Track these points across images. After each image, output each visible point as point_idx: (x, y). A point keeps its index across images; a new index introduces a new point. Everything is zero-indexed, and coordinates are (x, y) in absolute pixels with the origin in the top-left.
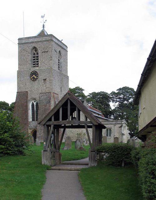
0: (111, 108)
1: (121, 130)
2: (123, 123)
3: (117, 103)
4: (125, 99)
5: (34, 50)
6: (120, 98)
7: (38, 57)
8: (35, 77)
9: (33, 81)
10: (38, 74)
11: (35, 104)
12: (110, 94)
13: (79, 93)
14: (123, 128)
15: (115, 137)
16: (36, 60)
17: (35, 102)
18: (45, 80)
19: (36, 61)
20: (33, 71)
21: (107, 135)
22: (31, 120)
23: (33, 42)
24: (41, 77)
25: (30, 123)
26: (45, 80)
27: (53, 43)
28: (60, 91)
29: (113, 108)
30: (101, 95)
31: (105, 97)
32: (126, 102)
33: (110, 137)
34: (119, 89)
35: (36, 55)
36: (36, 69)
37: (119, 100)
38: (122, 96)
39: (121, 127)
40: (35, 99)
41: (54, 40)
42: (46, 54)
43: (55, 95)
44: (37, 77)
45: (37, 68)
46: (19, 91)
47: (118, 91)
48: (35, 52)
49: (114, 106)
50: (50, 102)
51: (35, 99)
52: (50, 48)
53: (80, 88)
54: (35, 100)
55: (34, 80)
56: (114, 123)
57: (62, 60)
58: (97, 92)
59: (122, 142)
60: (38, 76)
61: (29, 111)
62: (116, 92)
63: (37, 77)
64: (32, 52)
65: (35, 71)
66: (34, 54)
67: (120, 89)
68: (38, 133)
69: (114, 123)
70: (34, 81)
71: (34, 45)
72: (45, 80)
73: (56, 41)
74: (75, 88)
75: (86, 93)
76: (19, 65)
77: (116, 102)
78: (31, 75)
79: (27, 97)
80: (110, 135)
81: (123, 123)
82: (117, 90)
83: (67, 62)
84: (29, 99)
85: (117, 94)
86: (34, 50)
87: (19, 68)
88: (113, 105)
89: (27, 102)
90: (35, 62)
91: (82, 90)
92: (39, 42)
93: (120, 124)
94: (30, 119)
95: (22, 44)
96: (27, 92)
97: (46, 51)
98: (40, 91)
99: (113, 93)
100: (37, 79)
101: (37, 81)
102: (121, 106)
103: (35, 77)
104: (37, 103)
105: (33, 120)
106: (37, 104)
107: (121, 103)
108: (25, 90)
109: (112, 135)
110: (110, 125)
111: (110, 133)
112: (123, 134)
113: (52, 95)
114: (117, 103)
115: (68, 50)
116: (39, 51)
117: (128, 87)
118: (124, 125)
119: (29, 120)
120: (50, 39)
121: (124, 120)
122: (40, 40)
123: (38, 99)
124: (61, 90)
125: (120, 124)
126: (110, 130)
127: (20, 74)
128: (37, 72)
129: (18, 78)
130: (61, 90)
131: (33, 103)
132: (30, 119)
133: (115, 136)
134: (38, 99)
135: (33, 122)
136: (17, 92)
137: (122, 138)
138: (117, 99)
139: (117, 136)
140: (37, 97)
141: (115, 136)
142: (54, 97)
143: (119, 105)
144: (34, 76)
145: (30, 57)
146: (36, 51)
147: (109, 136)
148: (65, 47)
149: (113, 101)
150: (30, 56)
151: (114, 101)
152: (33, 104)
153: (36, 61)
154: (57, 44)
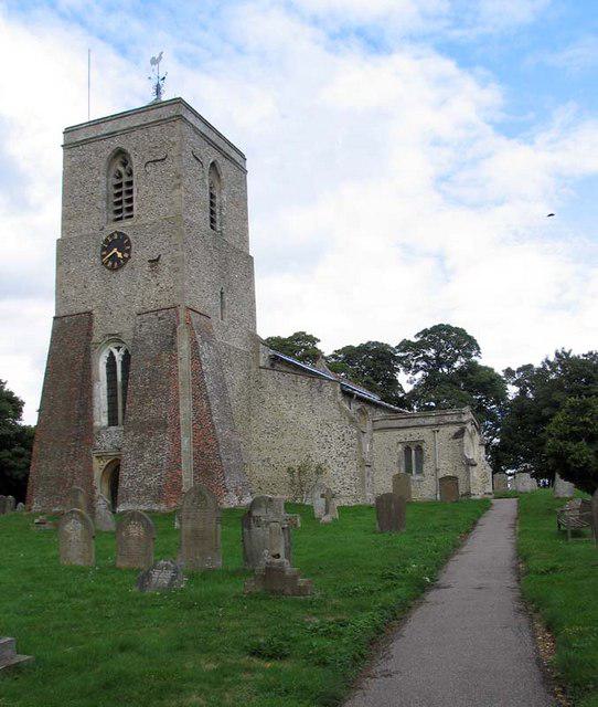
0: (401, 389)
1: (461, 445)
2: (465, 419)
3: (420, 375)
4: (440, 362)
5: (120, 159)
6: (426, 358)
7: (130, 183)
8: (120, 255)
9: (112, 269)
10: (129, 243)
11: (118, 356)
12: (397, 347)
13: (306, 348)
14: (466, 439)
15: (441, 475)
16: (125, 205)
17: (118, 349)
18: (154, 262)
19: (122, 200)
20: (112, 236)
21: (409, 470)
22: (104, 421)
23: (112, 134)
24: (140, 254)
25: (99, 433)
26: (154, 262)
27: (186, 128)
28: (216, 303)
29: (408, 388)
30: (370, 353)
31: (379, 358)
32: (446, 370)
33: (418, 477)
34: (421, 333)
35: (125, 179)
36: (125, 226)
37: (424, 363)
38: (433, 351)
39: (459, 435)
40: (116, 339)
41: (191, 119)
42: (160, 167)
43: (195, 318)
44: (126, 255)
45: (128, 223)
46: (62, 313)
47: (419, 339)
48: (121, 169)
49: (411, 382)
50: (173, 343)
51: (116, 339)
52: (174, 144)
53: (308, 333)
54: (119, 341)
55: (115, 265)
56: (432, 421)
57: (223, 198)
58: (356, 344)
59: (468, 494)
60: (129, 251)
61: (96, 386)
62: (415, 340)
63: (126, 255)
64: (109, 169)
65: (119, 234)
66: (120, 176)
67: (425, 332)
68: (124, 473)
69: (432, 421)
70: (116, 269)
71: (117, 143)
72: (157, 260)
73: (200, 126)
74: (292, 335)
75: (327, 347)
76: (63, 220)
77: (415, 372)
78: (103, 249)
79: (89, 335)
80: (420, 471)
81: (465, 419)
82: (418, 335)
83: (246, 208)
84: (97, 337)
85: (416, 345)
86: (120, 159)
87: (63, 228)
88: (406, 381)
89: (87, 351)
90: (120, 203)
91: (314, 340)
92: (131, 129)
93: (456, 423)
94: (101, 420)
95: (77, 144)
96: (90, 313)
97: (159, 158)
98: (137, 307)
99: (405, 345)
100: (125, 260)
101: (123, 273)
102: (430, 383)
103: (120, 255)
104: (126, 352)
105: (113, 421)
106: (127, 358)
107: (430, 371)
108: (82, 309)
109: (427, 467)
110: (420, 431)
111: (420, 462)
112: (470, 464)
113: (182, 314)
114: (420, 375)
115: (249, 166)
116: (135, 162)
117: (448, 326)
118: (470, 427)
119: (97, 423)
120: (173, 113)
121: (467, 409)
122: (138, 124)
123: (127, 337)
124: (222, 302)
125: (456, 423)
126: (419, 449)
127: (66, 250)
128: (125, 237)
129: (59, 264)
130: (222, 302)
131: (111, 353)
132: (101, 420)
133: (437, 470)
134: (127, 337)
135: (113, 428)
136: (55, 318)
137: (468, 479)
138: (417, 360)
139: (446, 469)
140: (125, 328)
141: (437, 470)
142: (189, 324)
143: (425, 378)
144: (116, 252)
145: (102, 185)
146: (124, 164)
147: (417, 473)
148: (234, 155)
149: (408, 368)
150: (103, 184)
151: (410, 368)
152: (111, 359)
153: (122, 200)
154: (203, 135)
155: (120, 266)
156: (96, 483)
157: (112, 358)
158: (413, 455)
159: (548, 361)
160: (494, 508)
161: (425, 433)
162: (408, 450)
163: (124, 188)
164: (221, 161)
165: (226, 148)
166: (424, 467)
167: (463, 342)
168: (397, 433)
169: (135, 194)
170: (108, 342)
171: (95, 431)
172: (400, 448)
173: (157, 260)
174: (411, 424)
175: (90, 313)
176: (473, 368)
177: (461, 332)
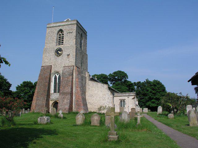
11: (57, 76)
16: (61, 40)
17: (58, 75)
22: (53, 92)
24: (65, 53)
36: (61, 46)
45: (62, 46)
48: (61, 33)
51: (58, 73)
57: (79, 46)
69: (128, 95)
71: (60, 28)
72: (69, 55)
84: (52, 72)
90: (60, 39)
97: (71, 32)
98: (63, 65)
105: (55, 91)
108: (48, 64)
116: (65, 33)
119: (51, 92)
126: (124, 101)
131: (56, 76)
132: (52, 90)
134: (61, 72)
148: (85, 32)
155: (60, 56)
156: (50, 107)
157: (56, 77)
158: (122, 102)
159: (145, 81)
160: (55, 44)
161: (126, 98)
162: (121, 101)
163: (61, 38)
164: (83, 33)
165: (84, 30)
166: (125, 105)
167: (124, 75)
168: (119, 97)
169: (64, 39)
170: (55, 73)
171: (51, 94)
172: (120, 101)
173: (69, 55)
174: (122, 95)
175: (51, 66)
176: (126, 81)
177: (123, 73)
